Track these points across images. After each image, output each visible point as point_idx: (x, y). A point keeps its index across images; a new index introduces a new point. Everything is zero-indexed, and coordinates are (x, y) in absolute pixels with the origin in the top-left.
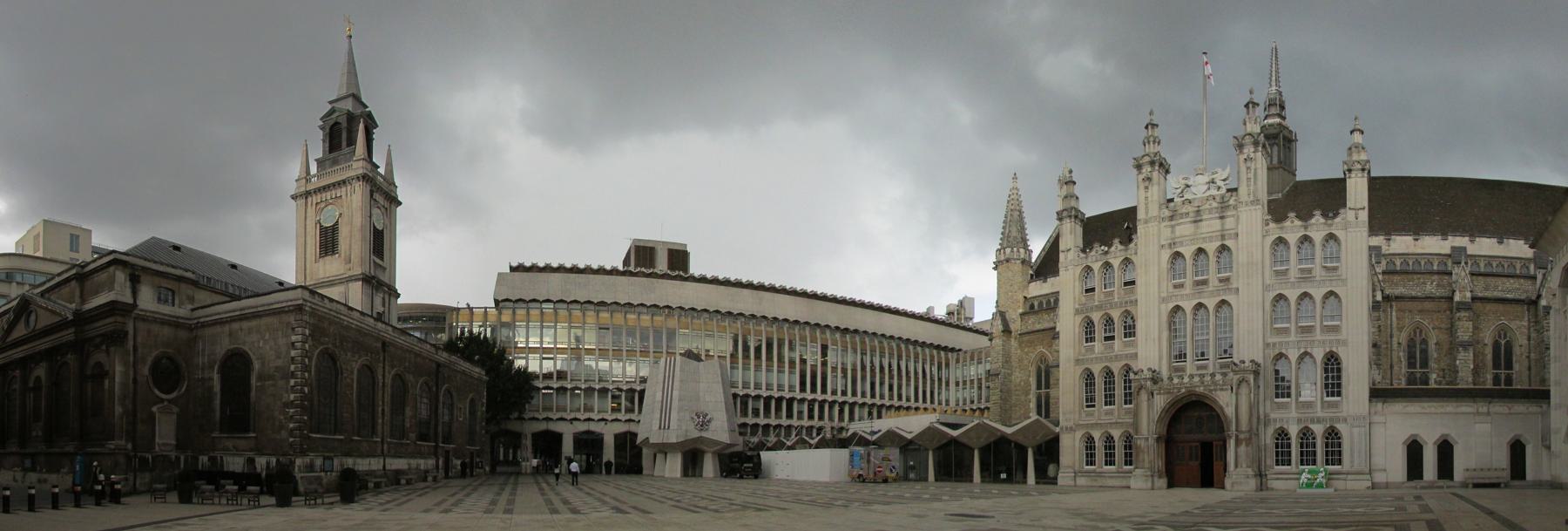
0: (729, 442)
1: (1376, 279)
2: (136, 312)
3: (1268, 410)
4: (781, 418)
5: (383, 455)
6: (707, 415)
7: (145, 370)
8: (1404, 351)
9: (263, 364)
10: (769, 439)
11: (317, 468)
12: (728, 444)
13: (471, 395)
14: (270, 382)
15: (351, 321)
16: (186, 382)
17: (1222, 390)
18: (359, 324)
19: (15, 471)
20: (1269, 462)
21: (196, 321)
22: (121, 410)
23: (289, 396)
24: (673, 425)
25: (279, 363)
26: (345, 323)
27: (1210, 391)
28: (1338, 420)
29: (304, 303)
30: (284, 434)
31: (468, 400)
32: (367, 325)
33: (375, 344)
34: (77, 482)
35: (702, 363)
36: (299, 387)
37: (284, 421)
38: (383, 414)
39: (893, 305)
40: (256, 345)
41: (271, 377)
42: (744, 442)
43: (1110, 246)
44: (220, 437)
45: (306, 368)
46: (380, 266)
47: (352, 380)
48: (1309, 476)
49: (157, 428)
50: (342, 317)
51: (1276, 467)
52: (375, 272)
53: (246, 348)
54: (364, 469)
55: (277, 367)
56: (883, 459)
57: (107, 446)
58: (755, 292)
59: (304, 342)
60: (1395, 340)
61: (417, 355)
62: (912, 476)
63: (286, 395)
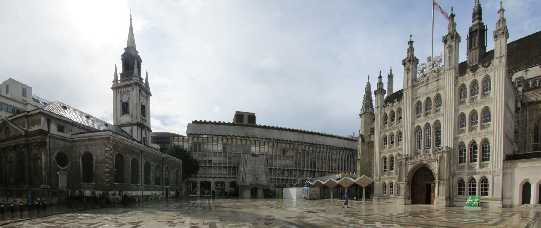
0: (266, 185)
2: (50, 134)
3: (455, 169)
4: (292, 176)
5: (142, 190)
6: (258, 176)
7: (54, 158)
9: (97, 157)
13: (176, 169)
17: (433, 161)
19: (3, 197)
20: (455, 193)
21: (72, 140)
22: (45, 173)
25: (102, 158)
26: (126, 144)
27: (429, 162)
28: (486, 172)
29: (110, 136)
30: (105, 183)
34: (29, 201)
35: (257, 158)
36: (109, 167)
37: (104, 179)
39: (330, 134)
40: (94, 151)
41: (100, 163)
45: (112, 160)
47: (129, 164)
49: (59, 180)
50: (125, 142)
52: (142, 122)
53: (91, 151)
54: (135, 195)
55: (101, 159)
59: (111, 151)
63: (105, 169)
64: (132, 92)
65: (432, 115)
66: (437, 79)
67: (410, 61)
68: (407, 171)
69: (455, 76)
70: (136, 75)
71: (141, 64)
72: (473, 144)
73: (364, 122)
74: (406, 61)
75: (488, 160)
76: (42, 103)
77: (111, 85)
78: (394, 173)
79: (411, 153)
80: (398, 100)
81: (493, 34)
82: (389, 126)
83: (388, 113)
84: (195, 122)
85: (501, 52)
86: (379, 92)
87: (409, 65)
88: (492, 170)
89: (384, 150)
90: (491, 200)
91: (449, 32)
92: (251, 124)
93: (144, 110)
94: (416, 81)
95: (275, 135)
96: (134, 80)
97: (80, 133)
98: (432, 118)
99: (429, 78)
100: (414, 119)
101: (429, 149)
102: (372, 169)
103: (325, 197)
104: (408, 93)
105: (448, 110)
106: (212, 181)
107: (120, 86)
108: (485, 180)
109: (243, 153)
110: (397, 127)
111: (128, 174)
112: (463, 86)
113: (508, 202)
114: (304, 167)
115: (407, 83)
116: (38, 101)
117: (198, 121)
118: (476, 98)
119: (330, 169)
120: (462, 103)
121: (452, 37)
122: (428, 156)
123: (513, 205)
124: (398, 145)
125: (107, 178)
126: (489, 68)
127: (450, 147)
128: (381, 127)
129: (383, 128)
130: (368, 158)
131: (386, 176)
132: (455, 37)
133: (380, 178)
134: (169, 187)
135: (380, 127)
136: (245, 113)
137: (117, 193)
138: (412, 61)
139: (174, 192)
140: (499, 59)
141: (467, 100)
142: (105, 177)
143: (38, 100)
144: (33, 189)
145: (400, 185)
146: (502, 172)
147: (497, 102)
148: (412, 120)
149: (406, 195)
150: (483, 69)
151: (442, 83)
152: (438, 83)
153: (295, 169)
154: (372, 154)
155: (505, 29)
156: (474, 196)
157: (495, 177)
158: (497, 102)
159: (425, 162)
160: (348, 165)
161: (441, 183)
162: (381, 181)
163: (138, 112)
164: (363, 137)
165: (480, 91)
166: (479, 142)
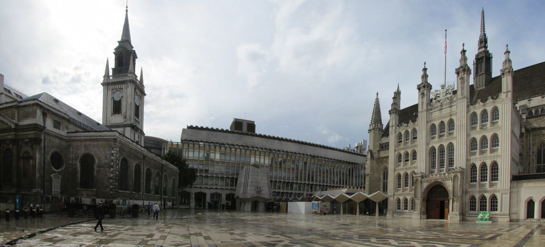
0: (269, 198)
1: (522, 122)
2: (45, 130)
3: (467, 188)
4: (288, 190)
5: (143, 199)
6: (261, 188)
7: (48, 158)
8: (535, 156)
9: (99, 161)
10: (284, 198)
11: (121, 204)
12: (268, 199)
13: (173, 177)
14: (103, 169)
15: (133, 146)
16: (65, 165)
17: (448, 180)
18: (136, 148)
20: (467, 209)
21: (69, 138)
22: (39, 175)
23: (110, 175)
24: (248, 192)
25: (106, 161)
27: (444, 180)
28: (496, 191)
30: (108, 190)
31: (173, 179)
32: (138, 148)
33: (141, 156)
35: (259, 169)
36: (115, 172)
37: (108, 185)
38: (143, 184)
41: (103, 167)
42: (274, 198)
43: (408, 123)
44: (81, 190)
45: (117, 165)
46: (137, 121)
47: (133, 170)
48: (482, 215)
50: (130, 145)
51: (470, 211)
52: (136, 124)
53: (92, 153)
55: (105, 163)
56: (324, 206)
57: (32, 191)
58: (280, 141)
60: (531, 151)
61: (155, 161)
62: (335, 212)
63: (109, 174)
64: (126, 91)
65: (445, 137)
66: (450, 105)
67: (424, 87)
68: (422, 188)
69: (467, 105)
70: (132, 72)
71: (136, 61)
72: (484, 166)
73: (373, 138)
74: (421, 86)
75: (497, 180)
76: (14, 94)
77: (102, 80)
78: (409, 190)
79: (426, 171)
80: (412, 121)
81: (501, 72)
82: (404, 145)
83: (403, 132)
84: (191, 128)
85: (507, 87)
86: (394, 112)
87: (424, 90)
88: (500, 189)
89: (399, 168)
90: (500, 215)
91: (461, 66)
92: (251, 133)
93: (138, 111)
94: (430, 105)
95: (276, 145)
96: (129, 77)
97: (77, 132)
98: (446, 140)
99: (443, 104)
100: (428, 140)
101: (434, 170)
102: (380, 185)
103: (335, 212)
104: (421, 116)
105: (461, 134)
106: (208, 192)
107: (112, 82)
108: (494, 198)
109: (242, 164)
110: (411, 146)
111: (131, 182)
112: (474, 114)
113: (514, 217)
114: (302, 180)
115: (422, 106)
116: (9, 92)
117: (194, 126)
118: (486, 125)
119: (332, 183)
120: (474, 128)
121: (464, 70)
122: (442, 175)
123: (519, 219)
124: (413, 163)
125: (111, 184)
126: (497, 100)
127: (463, 168)
128: (395, 146)
129: (397, 147)
130: (377, 173)
131: (400, 192)
132: (466, 70)
133: (394, 194)
134: (167, 197)
135: (395, 146)
136: (244, 120)
137: (121, 201)
138: (426, 87)
139: (171, 203)
140: (506, 94)
141: (478, 126)
142: (109, 184)
143: (9, 90)
144: (23, 192)
145: (416, 201)
146: (509, 191)
147: (504, 130)
148: (426, 141)
149: (421, 211)
150: (492, 100)
151: (455, 110)
152: (451, 110)
153: (296, 182)
154: (380, 170)
155: (511, 69)
156: (484, 212)
157: (504, 196)
158: (504, 130)
159: (440, 180)
160: (349, 179)
161: (455, 200)
162: (396, 197)
163: (131, 113)
164: (372, 152)
165: (489, 119)
166: (489, 163)
